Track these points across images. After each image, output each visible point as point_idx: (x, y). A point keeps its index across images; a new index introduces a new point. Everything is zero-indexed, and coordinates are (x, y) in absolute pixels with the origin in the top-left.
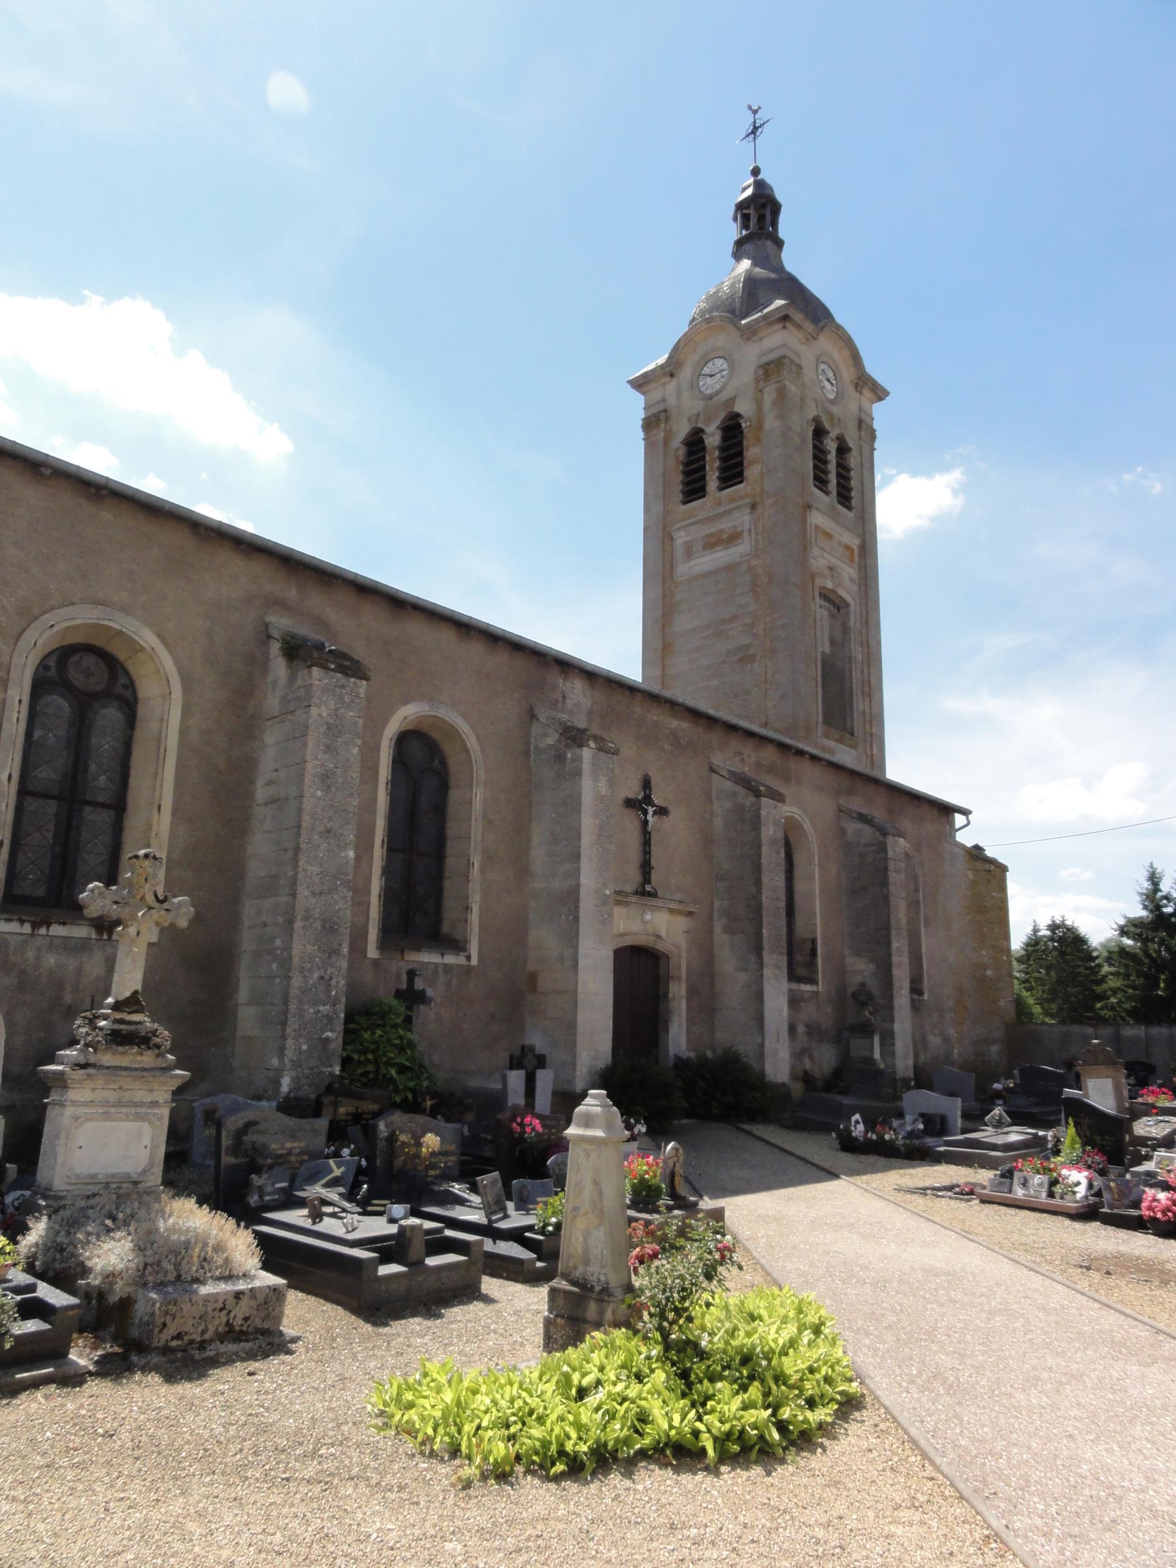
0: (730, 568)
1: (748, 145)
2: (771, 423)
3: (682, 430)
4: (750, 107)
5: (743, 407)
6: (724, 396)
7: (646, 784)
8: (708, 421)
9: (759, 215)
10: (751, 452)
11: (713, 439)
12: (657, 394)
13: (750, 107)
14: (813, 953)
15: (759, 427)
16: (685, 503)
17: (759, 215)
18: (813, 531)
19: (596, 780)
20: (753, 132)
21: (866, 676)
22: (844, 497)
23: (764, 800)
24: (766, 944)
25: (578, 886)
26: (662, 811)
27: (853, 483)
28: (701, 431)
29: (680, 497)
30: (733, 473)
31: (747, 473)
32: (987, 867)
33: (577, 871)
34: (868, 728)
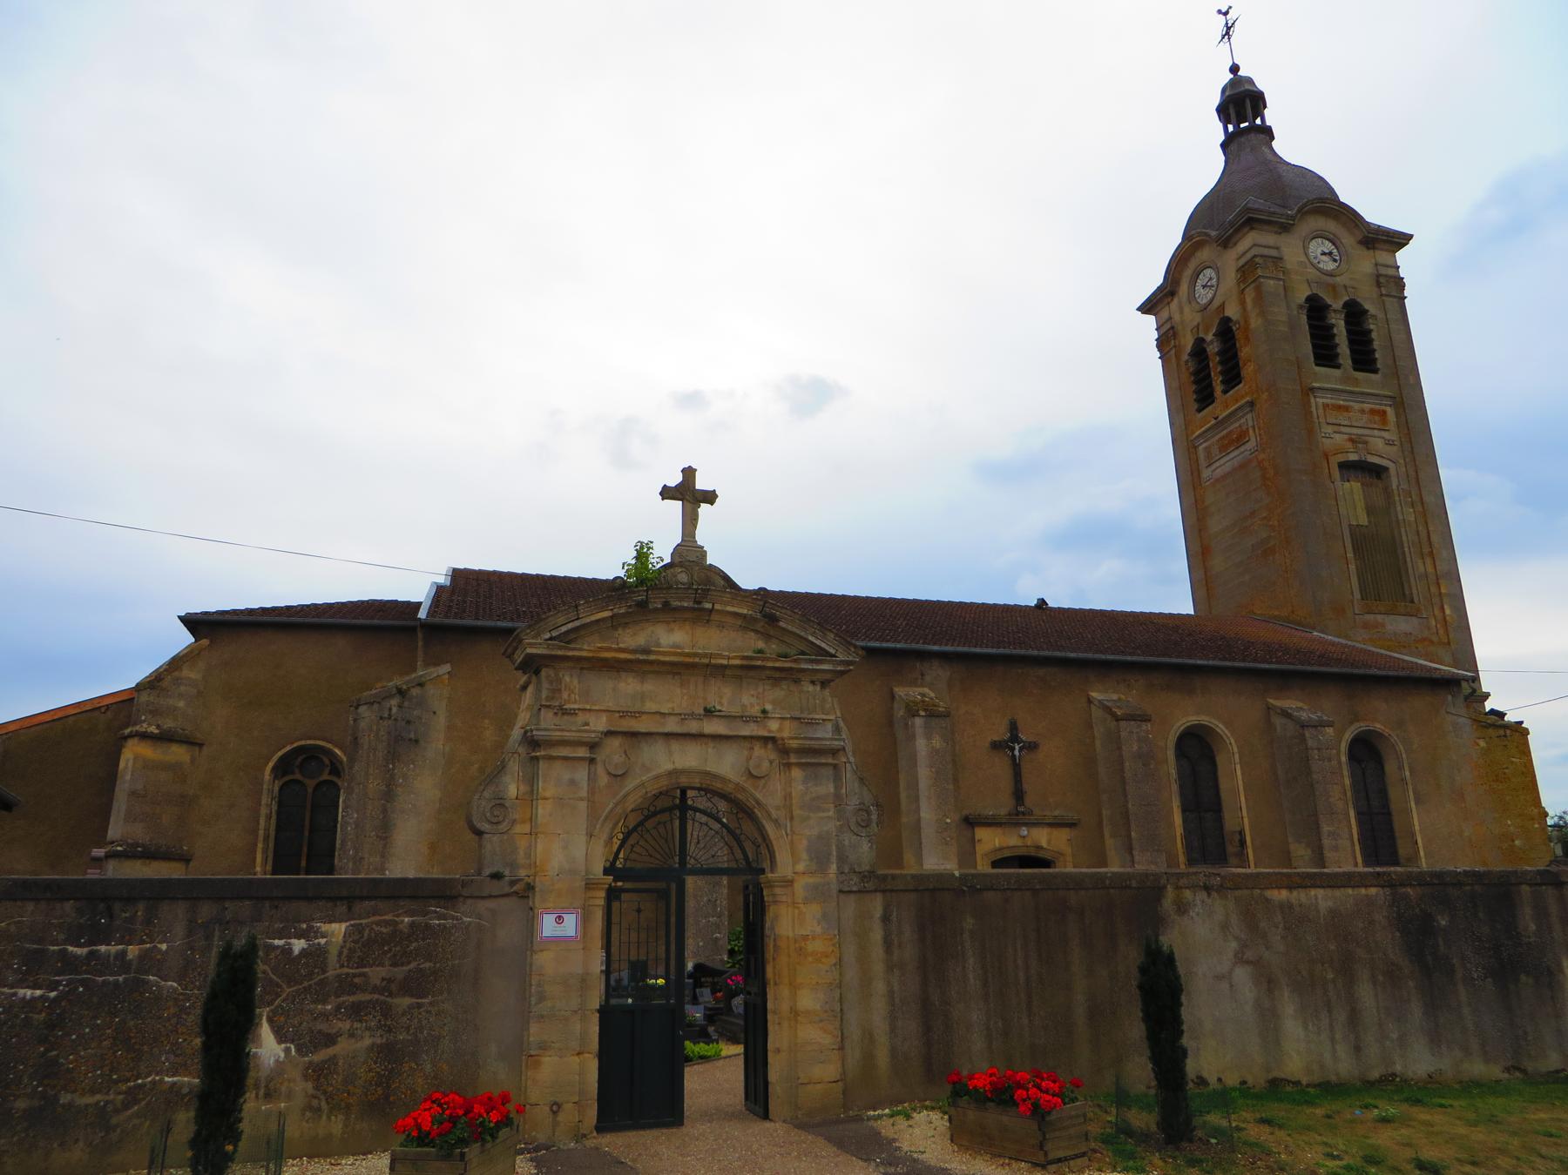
0: (1243, 466)
1: (1225, 46)
2: (1255, 322)
3: (1188, 343)
4: (1220, 12)
5: (1232, 312)
6: (1216, 303)
7: (1013, 727)
8: (1207, 331)
9: (1242, 105)
10: (1244, 352)
11: (1213, 348)
12: (1165, 314)
13: (1220, 12)
14: (1243, 843)
15: (1247, 329)
16: (1199, 410)
17: (1242, 105)
18: (1321, 411)
19: (929, 737)
20: (1229, 29)
21: (1424, 534)
22: (1364, 359)
23: (1123, 724)
24: (1136, 844)
25: (919, 820)
26: (1032, 747)
27: (1376, 345)
28: (1203, 340)
29: (1196, 406)
30: (1233, 377)
31: (1244, 373)
32: (1502, 732)
33: (918, 809)
34: (1433, 589)
